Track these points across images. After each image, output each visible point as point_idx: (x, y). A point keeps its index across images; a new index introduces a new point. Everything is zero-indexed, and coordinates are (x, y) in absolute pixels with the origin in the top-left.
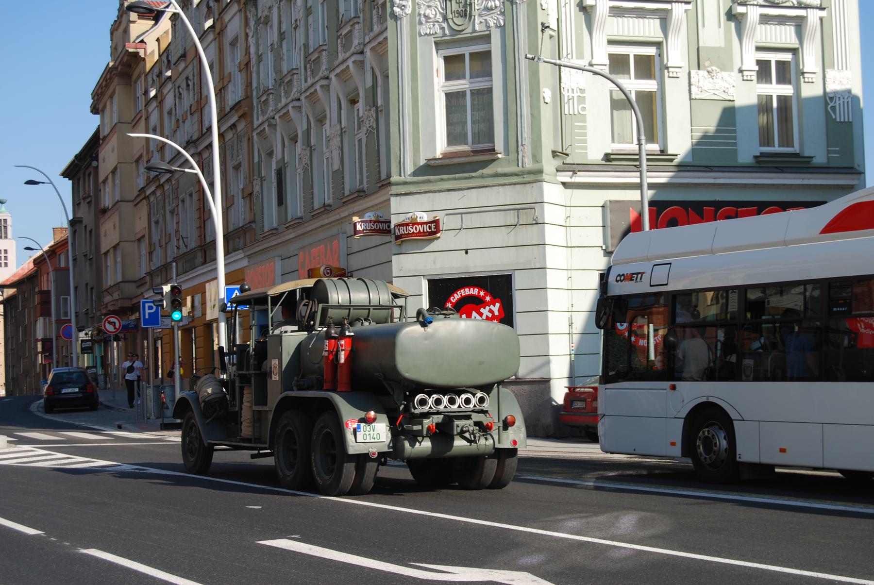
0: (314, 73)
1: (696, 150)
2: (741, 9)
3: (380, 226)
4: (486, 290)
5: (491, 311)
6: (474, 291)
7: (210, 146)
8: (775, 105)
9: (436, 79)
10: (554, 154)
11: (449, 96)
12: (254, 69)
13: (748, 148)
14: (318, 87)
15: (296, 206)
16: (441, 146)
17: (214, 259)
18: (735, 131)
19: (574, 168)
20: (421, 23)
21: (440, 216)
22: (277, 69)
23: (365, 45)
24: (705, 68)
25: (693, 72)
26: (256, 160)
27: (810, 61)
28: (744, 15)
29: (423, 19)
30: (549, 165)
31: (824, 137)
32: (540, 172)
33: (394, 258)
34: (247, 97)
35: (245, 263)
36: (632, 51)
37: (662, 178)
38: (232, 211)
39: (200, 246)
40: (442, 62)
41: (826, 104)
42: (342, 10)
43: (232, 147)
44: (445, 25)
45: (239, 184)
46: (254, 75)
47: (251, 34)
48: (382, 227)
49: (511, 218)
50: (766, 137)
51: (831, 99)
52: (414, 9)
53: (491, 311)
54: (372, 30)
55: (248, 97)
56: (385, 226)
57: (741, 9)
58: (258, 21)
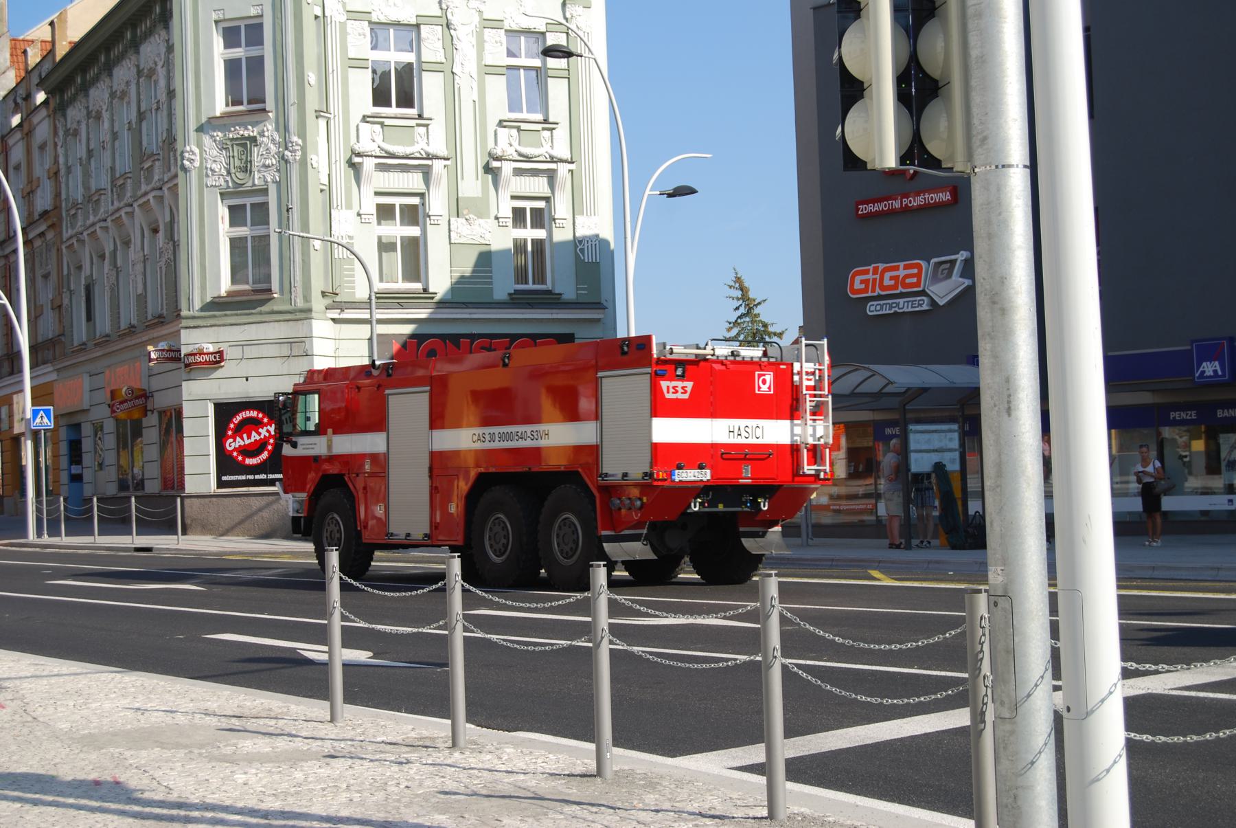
0: (120, 198)
1: (454, 289)
2: (495, 164)
3: (173, 354)
4: (264, 413)
5: (268, 431)
6: (254, 414)
7: (15, 251)
8: (529, 248)
9: (221, 226)
10: (324, 294)
11: (232, 240)
12: (63, 180)
13: (503, 286)
14: (122, 213)
15: (104, 323)
16: (225, 285)
17: (21, 371)
18: (491, 272)
19: (341, 306)
20: (207, 176)
21: (223, 347)
22: (87, 187)
23: (165, 183)
24: (463, 216)
25: (452, 220)
26: (65, 272)
27: (562, 208)
28: (499, 169)
29: (210, 173)
30: (318, 303)
31: (574, 277)
32: (310, 310)
33: (184, 384)
34: (56, 208)
35: (54, 376)
36: (398, 201)
37: (423, 314)
38: (41, 322)
39: (7, 355)
40: (226, 211)
41: (576, 247)
42: (145, 143)
43: (41, 255)
44: (228, 178)
45: (47, 295)
46: (63, 186)
47: (60, 144)
48: (173, 355)
49: (285, 350)
50: (521, 276)
51: (580, 242)
52: (201, 163)
53: (268, 431)
54: (169, 170)
55: (57, 207)
56: (177, 354)
57: (495, 164)
58: (67, 132)
